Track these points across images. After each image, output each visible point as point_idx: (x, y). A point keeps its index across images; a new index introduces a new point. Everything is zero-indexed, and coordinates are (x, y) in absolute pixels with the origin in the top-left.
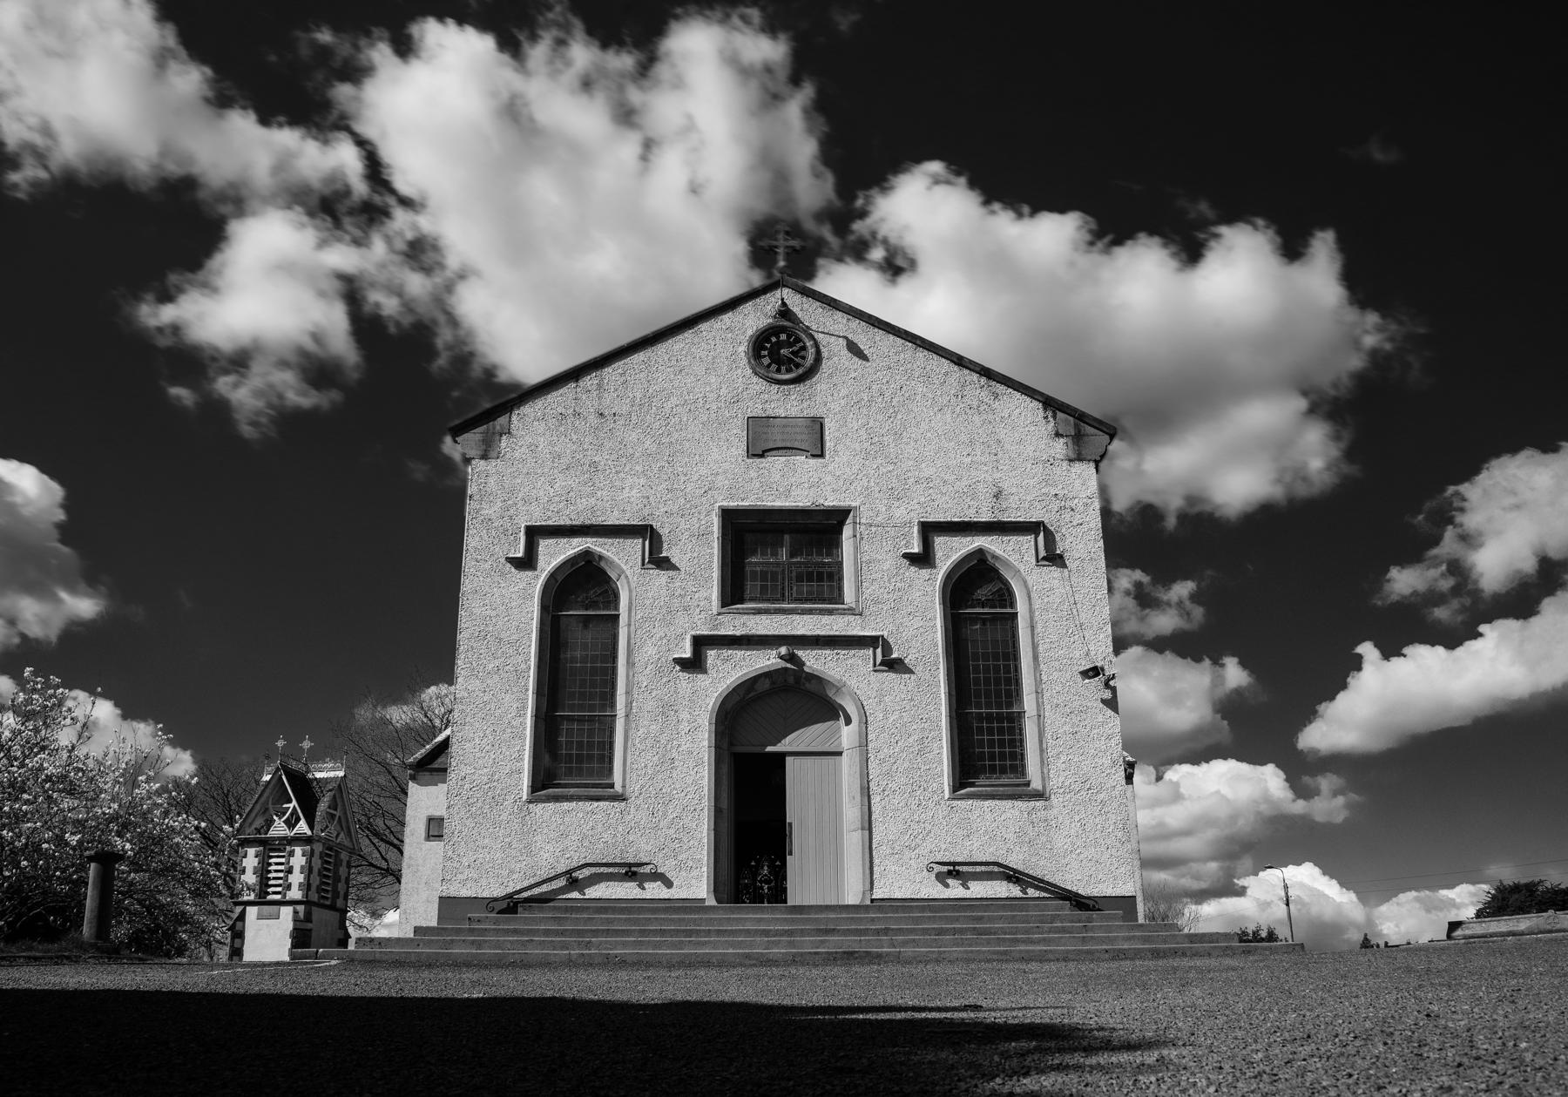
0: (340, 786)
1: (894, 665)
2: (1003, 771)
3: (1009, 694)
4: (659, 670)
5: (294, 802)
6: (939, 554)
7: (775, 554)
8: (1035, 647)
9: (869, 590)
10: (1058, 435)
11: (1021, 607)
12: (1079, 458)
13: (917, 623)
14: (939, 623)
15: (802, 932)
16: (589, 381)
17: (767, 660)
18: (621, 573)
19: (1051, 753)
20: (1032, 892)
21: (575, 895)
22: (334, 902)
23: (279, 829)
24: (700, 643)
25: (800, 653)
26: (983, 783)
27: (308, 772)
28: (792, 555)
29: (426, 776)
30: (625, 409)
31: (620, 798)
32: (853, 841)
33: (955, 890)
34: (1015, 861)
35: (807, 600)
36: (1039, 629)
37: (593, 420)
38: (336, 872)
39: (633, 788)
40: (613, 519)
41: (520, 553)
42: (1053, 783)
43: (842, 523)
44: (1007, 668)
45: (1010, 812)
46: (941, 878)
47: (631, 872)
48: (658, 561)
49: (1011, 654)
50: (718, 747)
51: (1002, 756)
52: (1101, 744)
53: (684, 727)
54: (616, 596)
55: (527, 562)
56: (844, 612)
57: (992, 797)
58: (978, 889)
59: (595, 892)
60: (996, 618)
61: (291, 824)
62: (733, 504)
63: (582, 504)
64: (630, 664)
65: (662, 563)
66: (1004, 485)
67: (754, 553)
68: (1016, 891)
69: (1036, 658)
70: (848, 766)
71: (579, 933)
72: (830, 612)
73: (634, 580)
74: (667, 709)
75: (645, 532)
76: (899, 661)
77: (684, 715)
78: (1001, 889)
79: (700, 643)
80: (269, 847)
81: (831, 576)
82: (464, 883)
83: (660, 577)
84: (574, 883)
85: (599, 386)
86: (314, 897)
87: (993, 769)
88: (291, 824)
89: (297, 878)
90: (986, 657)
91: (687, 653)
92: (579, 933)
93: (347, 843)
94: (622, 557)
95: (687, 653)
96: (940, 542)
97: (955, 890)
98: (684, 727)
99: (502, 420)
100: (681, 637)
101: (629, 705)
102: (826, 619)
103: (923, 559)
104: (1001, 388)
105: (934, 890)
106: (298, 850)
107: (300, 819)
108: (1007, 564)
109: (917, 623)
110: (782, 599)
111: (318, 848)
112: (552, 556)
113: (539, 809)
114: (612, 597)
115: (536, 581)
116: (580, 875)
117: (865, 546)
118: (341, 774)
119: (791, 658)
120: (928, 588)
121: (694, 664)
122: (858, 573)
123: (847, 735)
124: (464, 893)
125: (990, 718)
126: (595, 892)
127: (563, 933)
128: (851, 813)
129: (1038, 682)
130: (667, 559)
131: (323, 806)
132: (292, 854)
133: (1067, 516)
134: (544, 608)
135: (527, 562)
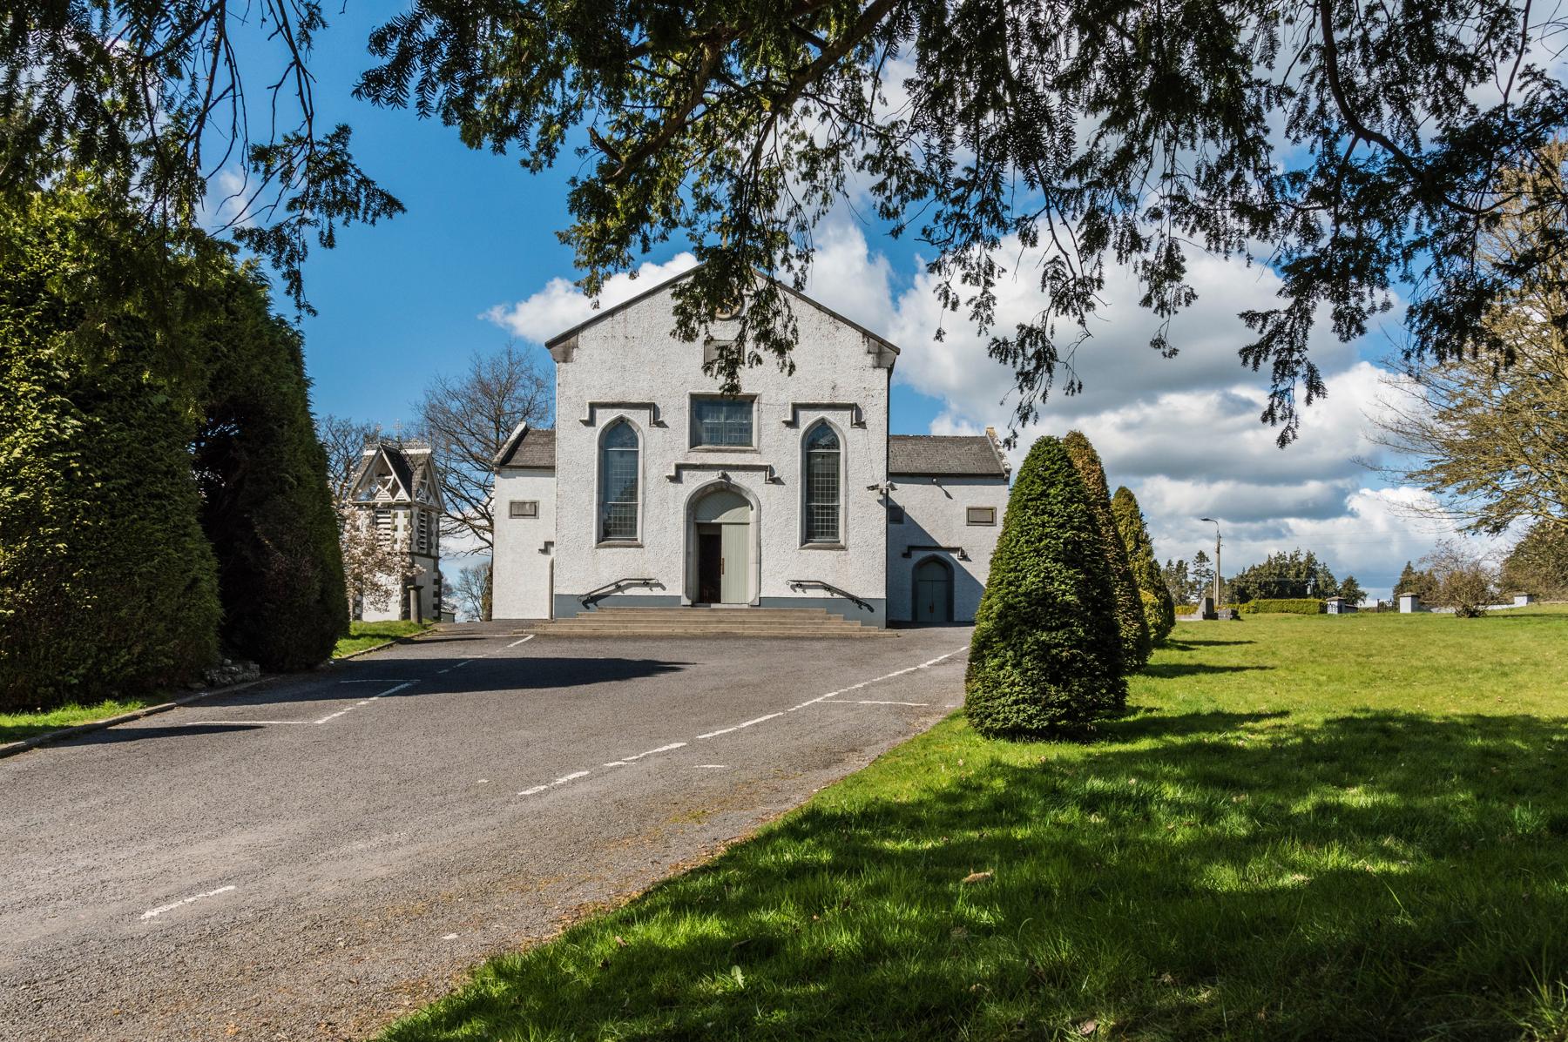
0: (429, 461)
1: (776, 481)
2: (828, 534)
3: (833, 495)
4: (659, 482)
5: (394, 475)
6: (801, 420)
7: (718, 418)
8: (846, 472)
9: (764, 440)
10: (869, 352)
11: (842, 450)
12: (879, 366)
13: (788, 458)
14: (799, 458)
15: (711, 622)
16: (619, 316)
17: (713, 477)
18: (639, 429)
19: (851, 527)
20: (836, 596)
21: (619, 593)
22: (429, 551)
23: (383, 497)
24: (679, 468)
25: (729, 473)
26: (817, 541)
27: (401, 447)
28: (727, 418)
29: (507, 472)
30: (639, 334)
31: (640, 546)
32: (753, 568)
33: (799, 594)
34: (829, 582)
35: (734, 444)
36: (849, 462)
37: (622, 340)
38: (429, 528)
39: (647, 542)
40: (634, 400)
41: (586, 418)
42: (851, 542)
43: (752, 402)
44: (833, 482)
45: (829, 556)
46: (793, 587)
47: (646, 583)
48: (658, 423)
49: (835, 475)
50: (688, 522)
51: (828, 527)
52: (875, 523)
53: (671, 511)
54: (637, 440)
55: (590, 422)
56: (752, 451)
57: (820, 548)
58: (811, 593)
59: (628, 592)
60: (829, 455)
61: (394, 490)
62: (696, 391)
63: (618, 390)
64: (644, 478)
65: (661, 424)
66: (838, 382)
67: (707, 417)
68: (828, 595)
69: (846, 478)
70: (752, 529)
71: (623, 622)
72: (745, 452)
73: (646, 433)
74: (663, 501)
75: (651, 407)
76: (779, 479)
77: (671, 505)
78: (822, 594)
79: (679, 468)
80: (378, 511)
81: (746, 431)
82: (566, 587)
83: (659, 431)
84: (619, 588)
85: (625, 320)
86: (415, 549)
87: (822, 533)
88: (394, 490)
89: (401, 534)
90: (823, 475)
91: (673, 473)
92: (623, 622)
93: (435, 504)
94: (640, 419)
95: (673, 473)
96: (802, 414)
97: (799, 594)
98: (671, 511)
99: (573, 339)
100: (669, 464)
101: (644, 500)
102: (743, 455)
103: (793, 424)
104: (841, 324)
105: (790, 594)
106: (401, 513)
107: (399, 488)
108: (836, 427)
109: (788, 458)
110: (720, 444)
111: (416, 511)
112: (603, 419)
113: (602, 551)
114: (635, 442)
115: (594, 433)
116: (622, 584)
117: (764, 416)
118: (428, 451)
119: (724, 476)
120: (795, 438)
121: (676, 479)
122: (759, 431)
123: (752, 515)
124: (566, 593)
125: (823, 507)
126: (628, 592)
127: (615, 621)
128: (752, 555)
129: (847, 490)
130: (662, 422)
131: (417, 478)
132: (395, 516)
133: (869, 399)
134: (600, 447)
135: (590, 422)
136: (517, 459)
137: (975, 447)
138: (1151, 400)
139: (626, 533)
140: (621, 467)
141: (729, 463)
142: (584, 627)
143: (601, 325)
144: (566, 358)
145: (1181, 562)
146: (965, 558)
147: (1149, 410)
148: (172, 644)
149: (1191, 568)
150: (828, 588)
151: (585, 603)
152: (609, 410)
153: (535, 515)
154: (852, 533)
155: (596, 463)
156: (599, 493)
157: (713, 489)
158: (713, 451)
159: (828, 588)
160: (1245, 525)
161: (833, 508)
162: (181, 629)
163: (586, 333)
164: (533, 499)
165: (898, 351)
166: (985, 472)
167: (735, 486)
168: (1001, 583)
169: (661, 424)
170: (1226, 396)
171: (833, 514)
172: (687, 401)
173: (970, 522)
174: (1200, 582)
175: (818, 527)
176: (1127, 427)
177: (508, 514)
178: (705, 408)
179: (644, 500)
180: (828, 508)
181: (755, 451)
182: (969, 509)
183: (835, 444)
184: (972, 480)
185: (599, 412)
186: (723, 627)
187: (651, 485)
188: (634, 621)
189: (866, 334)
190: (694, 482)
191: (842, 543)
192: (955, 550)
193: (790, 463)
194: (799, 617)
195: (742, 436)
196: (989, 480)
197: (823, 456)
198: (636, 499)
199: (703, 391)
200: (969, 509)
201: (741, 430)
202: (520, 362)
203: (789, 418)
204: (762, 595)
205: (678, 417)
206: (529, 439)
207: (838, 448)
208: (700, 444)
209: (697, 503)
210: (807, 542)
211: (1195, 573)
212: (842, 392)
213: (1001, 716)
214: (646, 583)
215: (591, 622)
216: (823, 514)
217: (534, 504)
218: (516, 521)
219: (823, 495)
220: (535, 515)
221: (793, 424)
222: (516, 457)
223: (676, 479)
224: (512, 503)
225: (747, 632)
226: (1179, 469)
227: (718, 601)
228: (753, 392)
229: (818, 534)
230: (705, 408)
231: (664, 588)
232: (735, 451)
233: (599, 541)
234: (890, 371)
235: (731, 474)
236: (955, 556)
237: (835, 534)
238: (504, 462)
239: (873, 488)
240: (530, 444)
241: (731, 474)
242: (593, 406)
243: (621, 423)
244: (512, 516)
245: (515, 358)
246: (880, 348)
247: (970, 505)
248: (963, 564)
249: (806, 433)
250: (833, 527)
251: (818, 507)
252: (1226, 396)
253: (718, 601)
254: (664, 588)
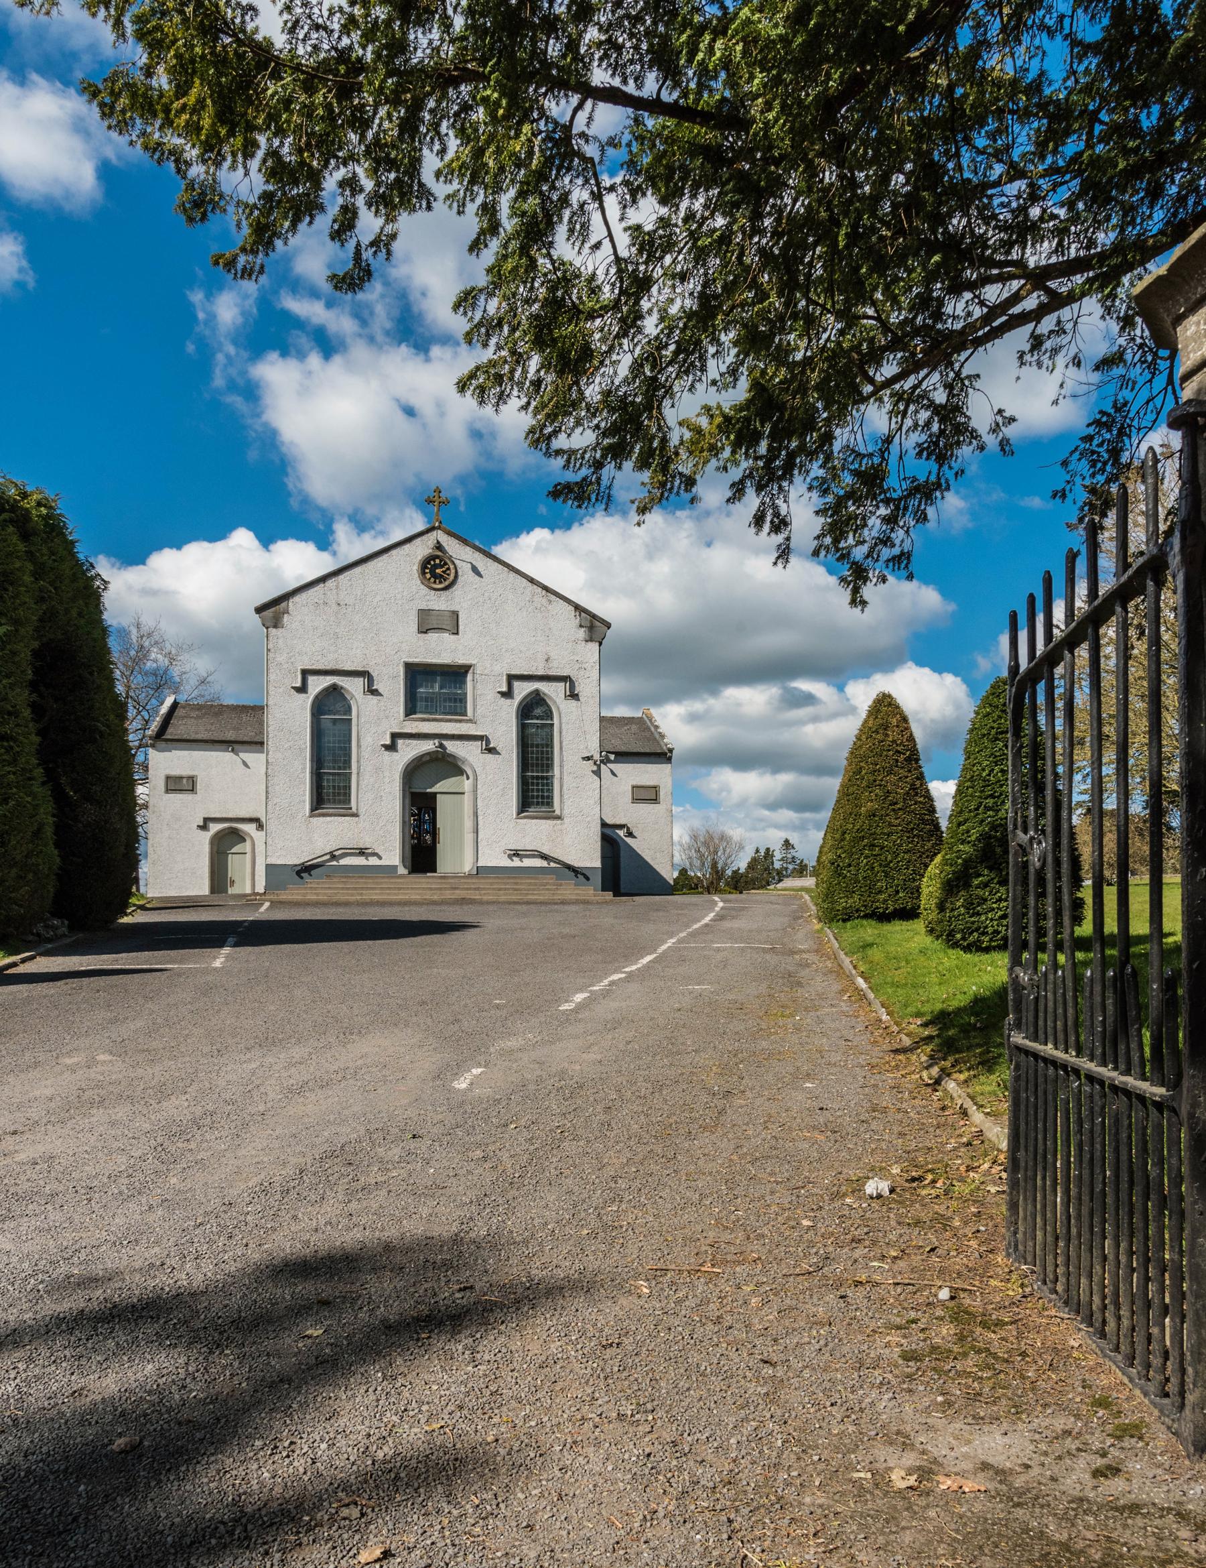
1: (491, 750)
2: (543, 803)
3: (548, 765)
8: (561, 743)
10: (581, 626)
11: (556, 721)
12: (590, 640)
14: (514, 729)
17: (429, 746)
18: (353, 696)
19: (566, 797)
20: (553, 865)
21: (334, 863)
24: (395, 736)
25: (445, 743)
28: (441, 688)
29: (162, 745)
31: (356, 815)
32: (469, 838)
33: (516, 863)
34: (545, 850)
36: (564, 733)
37: (335, 607)
39: (362, 811)
41: (298, 684)
42: (566, 812)
43: (467, 672)
45: (545, 825)
46: (510, 857)
47: (362, 852)
49: (549, 744)
53: (387, 780)
58: (528, 863)
59: (343, 862)
60: (544, 725)
62: (411, 660)
64: (359, 746)
65: (374, 692)
66: (553, 655)
67: (421, 686)
68: (544, 864)
69: (561, 748)
70: (467, 799)
71: (355, 889)
72: (460, 721)
73: (360, 701)
74: (378, 770)
76: (494, 749)
77: (387, 774)
78: (538, 863)
79: (395, 736)
81: (461, 701)
82: (278, 857)
84: (333, 857)
85: (337, 587)
87: (538, 803)
90: (537, 746)
91: (388, 742)
94: (354, 687)
95: (388, 742)
97: (516, 863)
98: (387, 780)
99: (284, 605)
101: (359, 768)
103: (508, 694)
104: (553, 597)
105: (506, 862)
110: (436, 713)
114: (348, 710)
115: (308, 700)
116: (337, 853)
117: (479, 686)
119: (441, 746)
120: (509, 709)
121: (391, 747)
123: (467, 785)
124: (279, 862)
125: (537, 778)
126: (343, 862)
128: (468, 824)
129: (562, 761)
133: (582, 672)
134: (313, 715)
135: (302, 689)
136: (171, 733)
137: (634, 727)
138: (714, 693)
139: (340, 802)
140: (334, 735)
141: (444, 732)
142: (317, 894)
143: (312, 592)
144: (276, 623)
145: (768, 849)
146: (630, 834)
147: (712, 701)
148: (22, 891)
149: (778, 855)
150: (544, 857)
151: (299, 873)
152: (321, 678)
153: (193, 790)
154: (567, 803)
155: (308, 730)
156: (312, 760)
157: (428, 758)
158: (428, 720)
159: (544, 857)
160: (807, 815)
161: (547, 778)
162: (30, 876)
163: (297, 599)
164: (191, 773)
165: (608, 626)
166: (648, 751)
167: (451, 755)
168: (977, 809)
169: (374, 692)
170: (787, 690)
171: (547, 784)
172: (401, 670)
173: (636, 800)
174: (786, 869)
175: (533, 797)
176: (693, 718)
177: (163, 789)
178: (419, 677)
179: (359, 768)
180: (543, 778)
181: (470, 721)
182: (633, 787)
183: (549, 715)
184: (636, 758)
185: (311, 679)
186: (459, 894)
187: (365, 754)
188: (367, 888)
189: (578, 608)
190: (410, 751)
191: (558, 812)
192: (621, 827)
193: (506, 734)
194: (530, 884)
195: (456, 706)
196: (652, 758)
197: (537, 726)
198: (350, 768)
199: (417, 660)
200: (633, 787)
201: (455, 701)
202: (150, 635)
203: (504, 689)
204: (480, 864)
205: (393, 686)
206: (179, 712)
207: (552, 719)
208: (415, 713)
209: (413, 771)
210: (523, 812)
211: (782, 859)
212: (555, 664)
213: (990, 930)
214: (362, 852)
215: (294, 893)
216: (538, 784)
217: (192, 779)
218: (171, 796)
219: (537, 765)
220: (193, 790)
221: (508, 694)
222: (170, 730)
223: (391, 747)
224: (168, 778)
225: (485, 898)
226: (743, 760)
227: (435, 871)
228: (461, 660)
229: (533, 803)
230: (419, 677)
231: (380, 858)
232: (450, 721)
233: (313, 809)
234: (600, 644)
235: (445, 742)
236: (621, 833)
237: (550, 803)
238: (160, 735)
239: (588, 758)
240: (183, 718)
241: (445, 742)
242: (305, 673)
243: (334, 690)
244: (167, 791)
245: (144, 630)
246: (591, 622)
247: (635, 783)
248: (629, 840)
249: (520, 703)
250: (548, 797)
251: (533, 777)
252: (787, 690)
253: (435, 871)
254: (380, 858)
